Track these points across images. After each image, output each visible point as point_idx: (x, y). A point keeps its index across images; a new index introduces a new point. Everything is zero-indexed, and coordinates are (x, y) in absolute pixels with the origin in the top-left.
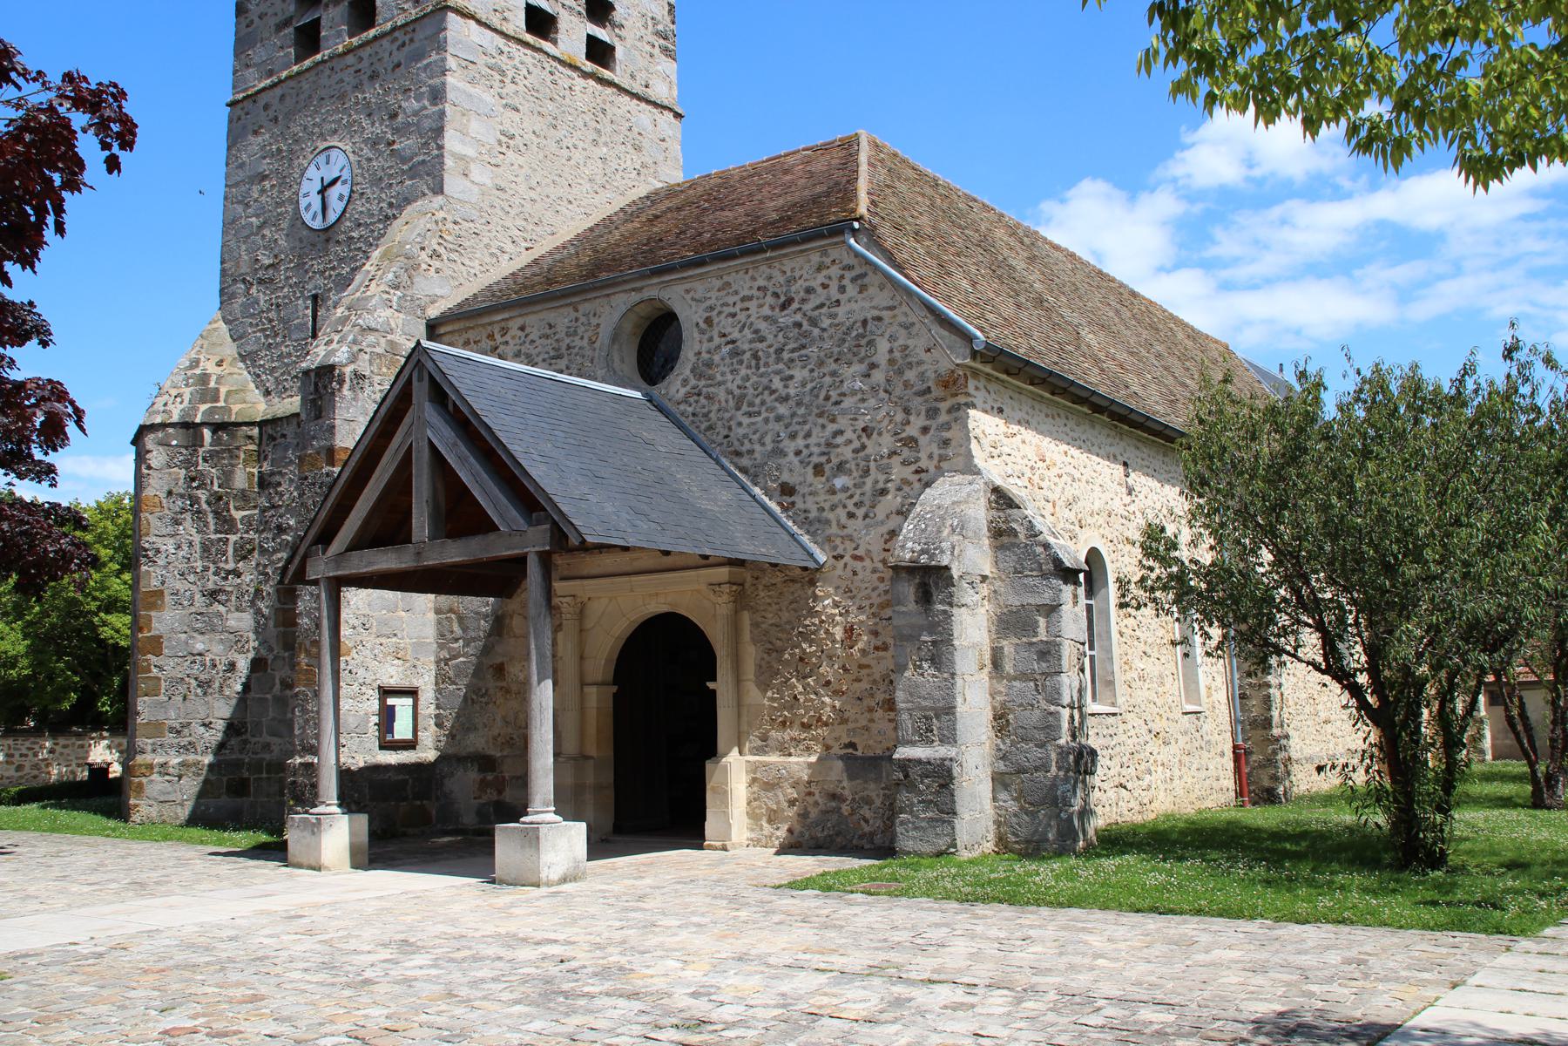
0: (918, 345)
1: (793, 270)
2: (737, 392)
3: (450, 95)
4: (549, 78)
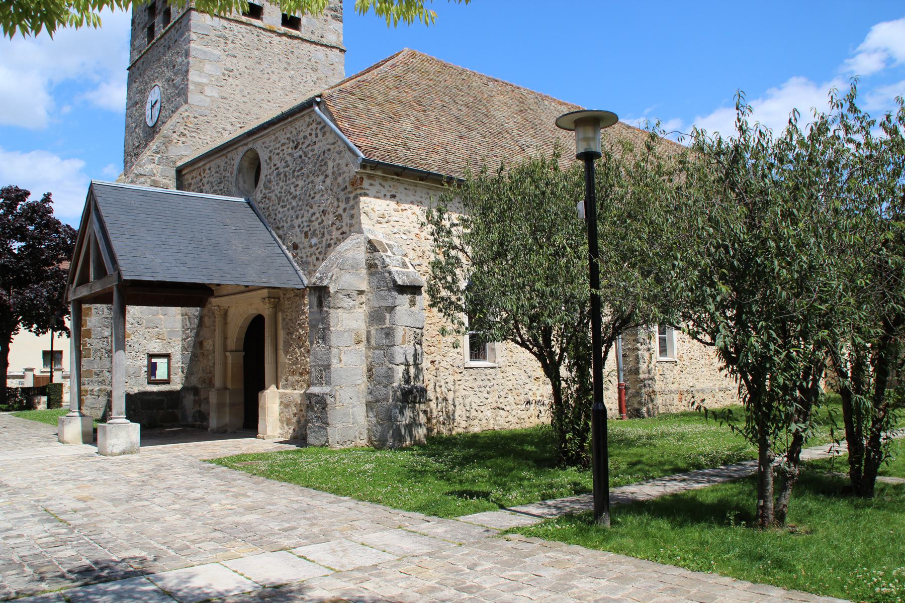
2: (279, 195)
3: (192, 53)
4: (256, 39)
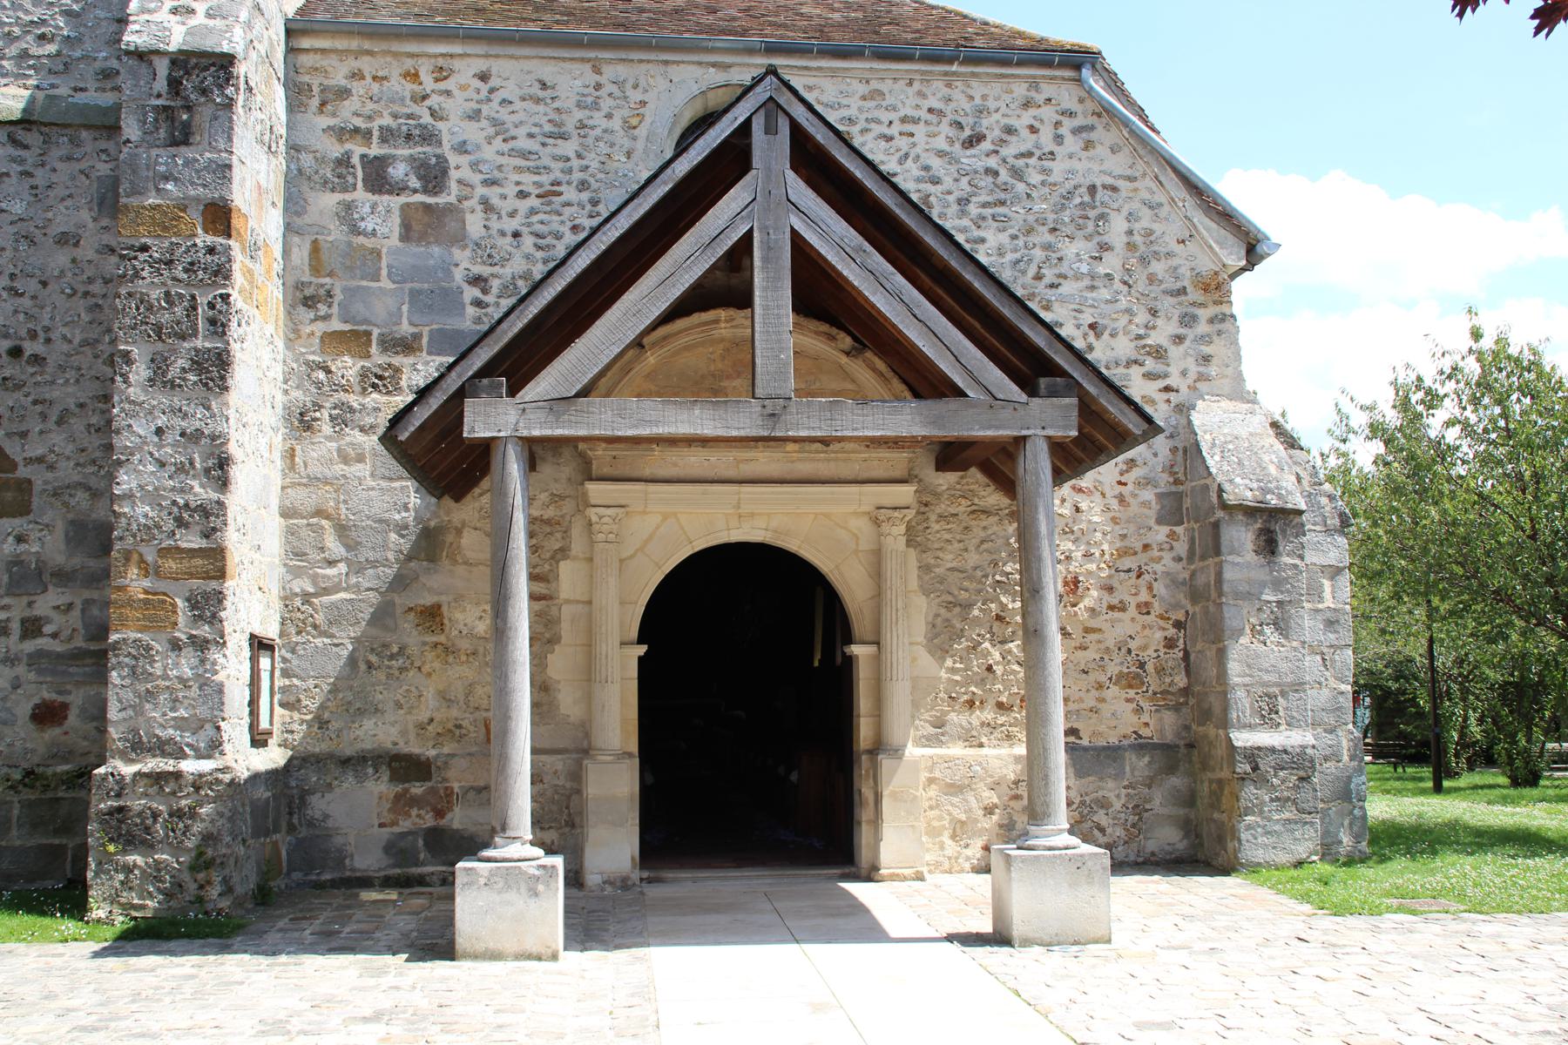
0: (1169, 231)
1: (984, 97)
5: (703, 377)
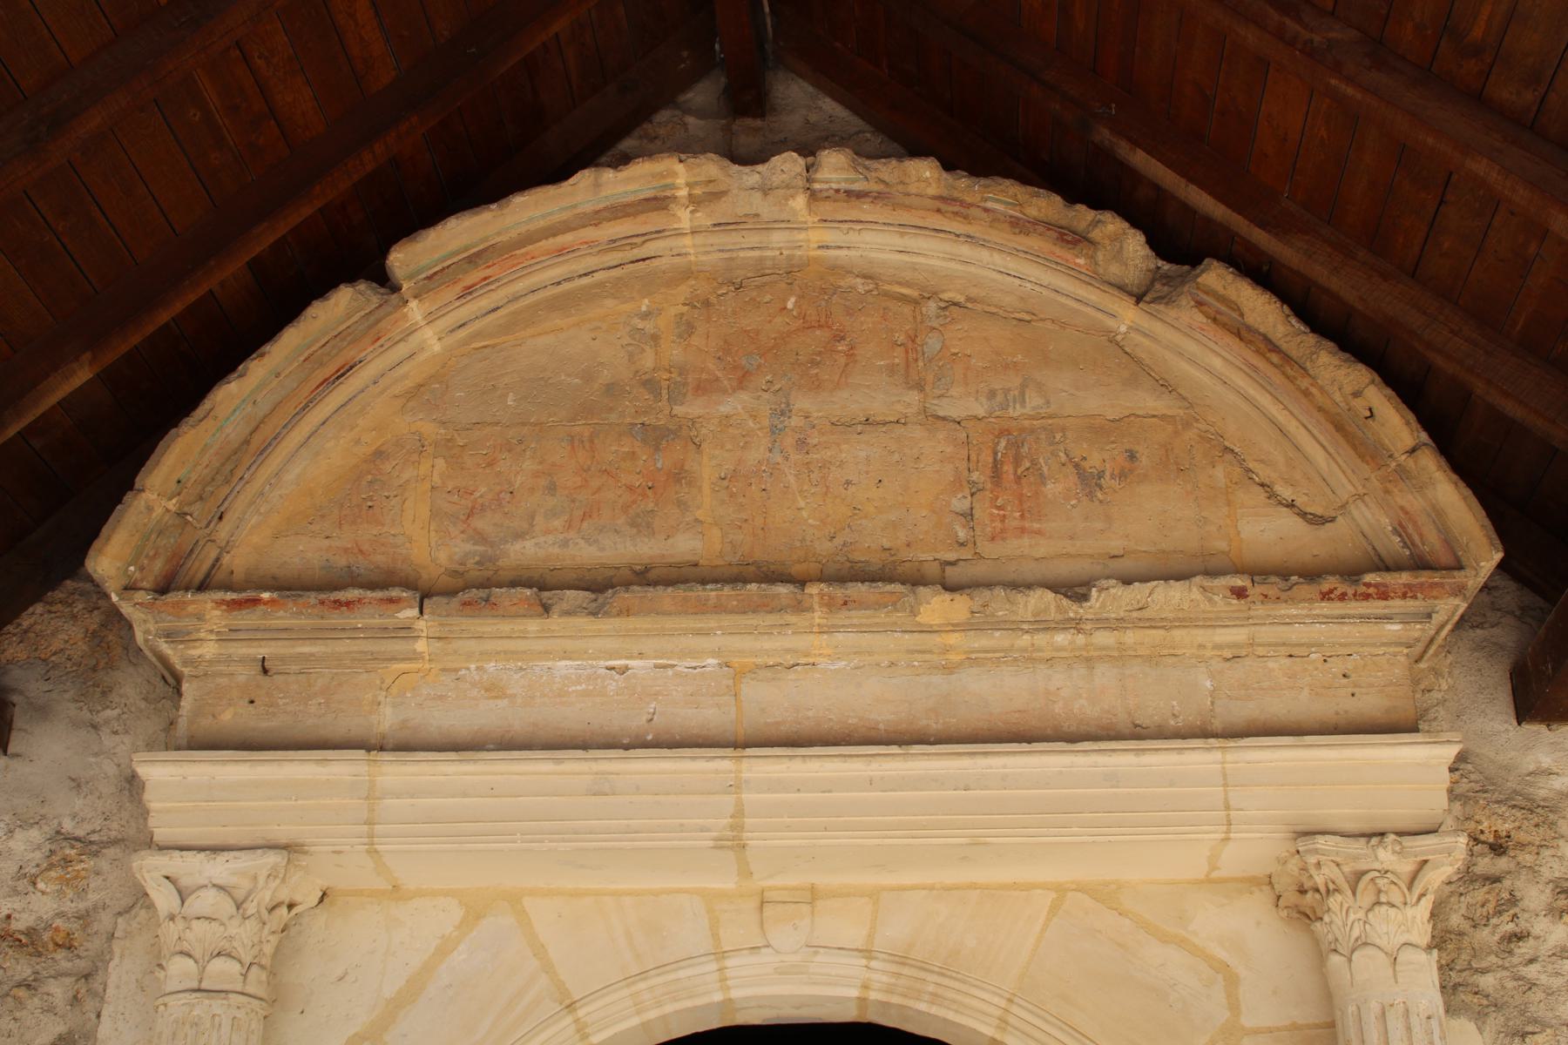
5: (612, 389)
